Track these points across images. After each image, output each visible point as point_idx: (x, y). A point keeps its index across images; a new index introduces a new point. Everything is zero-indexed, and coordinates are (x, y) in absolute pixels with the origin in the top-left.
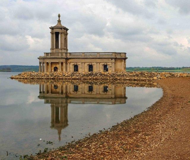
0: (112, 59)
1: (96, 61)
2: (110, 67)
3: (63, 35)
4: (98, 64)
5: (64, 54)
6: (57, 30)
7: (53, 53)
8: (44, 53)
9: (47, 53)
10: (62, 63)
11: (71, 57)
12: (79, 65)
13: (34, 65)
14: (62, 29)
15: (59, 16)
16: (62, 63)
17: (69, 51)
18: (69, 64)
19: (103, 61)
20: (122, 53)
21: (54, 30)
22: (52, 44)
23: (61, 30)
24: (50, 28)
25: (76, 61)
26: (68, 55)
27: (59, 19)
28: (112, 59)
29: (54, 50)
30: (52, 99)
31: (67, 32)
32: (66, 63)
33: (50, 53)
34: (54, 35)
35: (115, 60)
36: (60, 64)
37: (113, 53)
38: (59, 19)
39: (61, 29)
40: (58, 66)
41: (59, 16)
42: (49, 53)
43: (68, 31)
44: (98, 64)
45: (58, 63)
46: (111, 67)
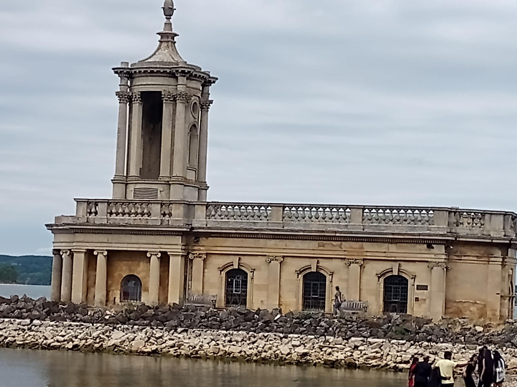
0: (430, 246)
1: (341, 254)
2: (419, 287)
3: (180, 107)
4: (355, 267)
5: (178, 212)
6: (150, 80)
7: (125, 202)
8: (79, 201)
9: (88, 202)
10: (165, 258)
11: (212, 223)
12: (253, 271)
13: (174, 167)
14: (177, 78)
15: (169, 11)
16: (165, 258)
17: (211, 197)
18: (198, 263)
19: (381, 256)
20: (492, 214)
21: (138, 81)
22: (130, 132)
23: (172, 81)
24: (116, 71)
25: (241, 251)
26: (200, 213)
27: (168, 25)
28: (430, 246)
29: (131, 188)
30: (126, 67)
31: (205, 94)
32: (188, 262)
33: (108, 202)
34: (137, 107)
35: (448, 252)
36: (155, 261)
37: (440, 209)
38: (168, 25)
39: (173, 75)
40: (140, 271)
41: (169, 11)
42: (103, 201)
43: (211, 89)
44: (355, 267)
45: (142, 255)
46: (425, 288)
